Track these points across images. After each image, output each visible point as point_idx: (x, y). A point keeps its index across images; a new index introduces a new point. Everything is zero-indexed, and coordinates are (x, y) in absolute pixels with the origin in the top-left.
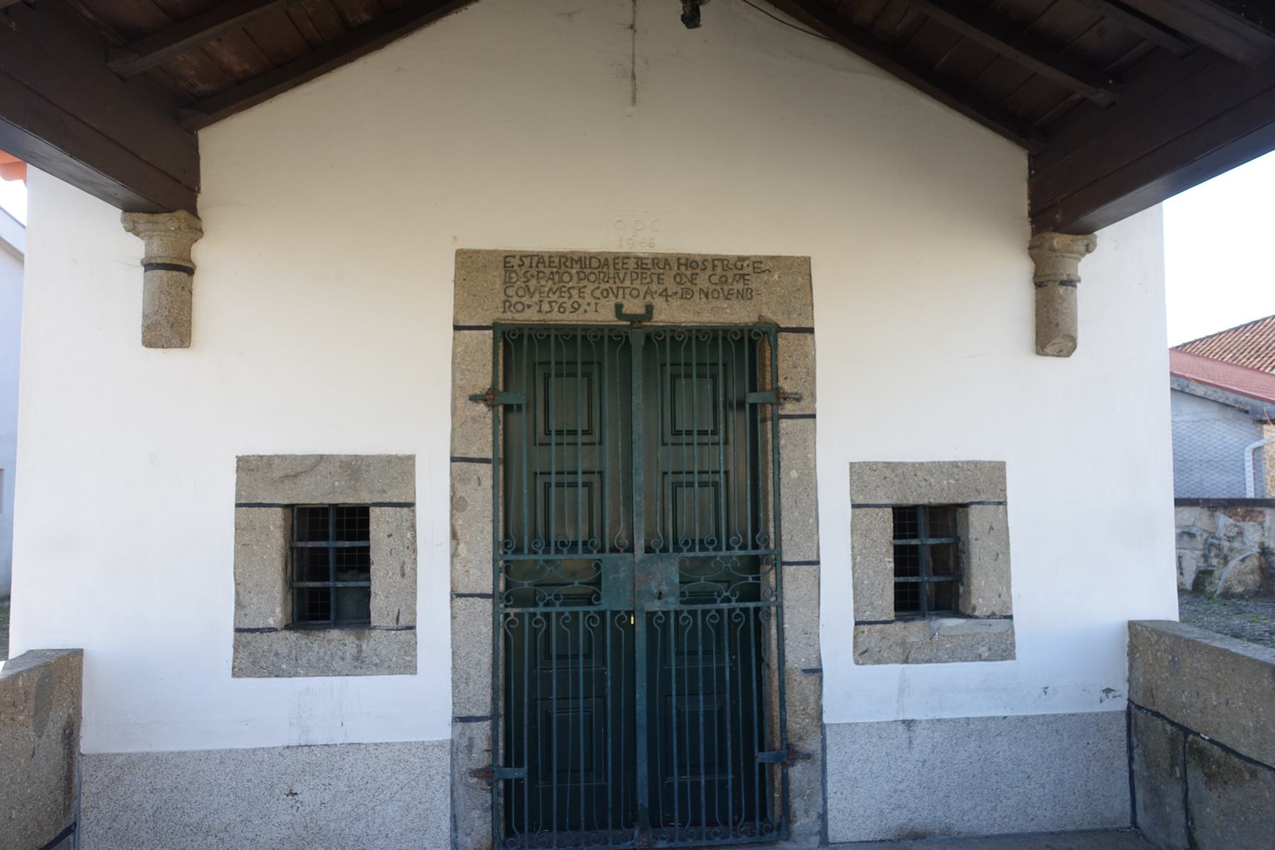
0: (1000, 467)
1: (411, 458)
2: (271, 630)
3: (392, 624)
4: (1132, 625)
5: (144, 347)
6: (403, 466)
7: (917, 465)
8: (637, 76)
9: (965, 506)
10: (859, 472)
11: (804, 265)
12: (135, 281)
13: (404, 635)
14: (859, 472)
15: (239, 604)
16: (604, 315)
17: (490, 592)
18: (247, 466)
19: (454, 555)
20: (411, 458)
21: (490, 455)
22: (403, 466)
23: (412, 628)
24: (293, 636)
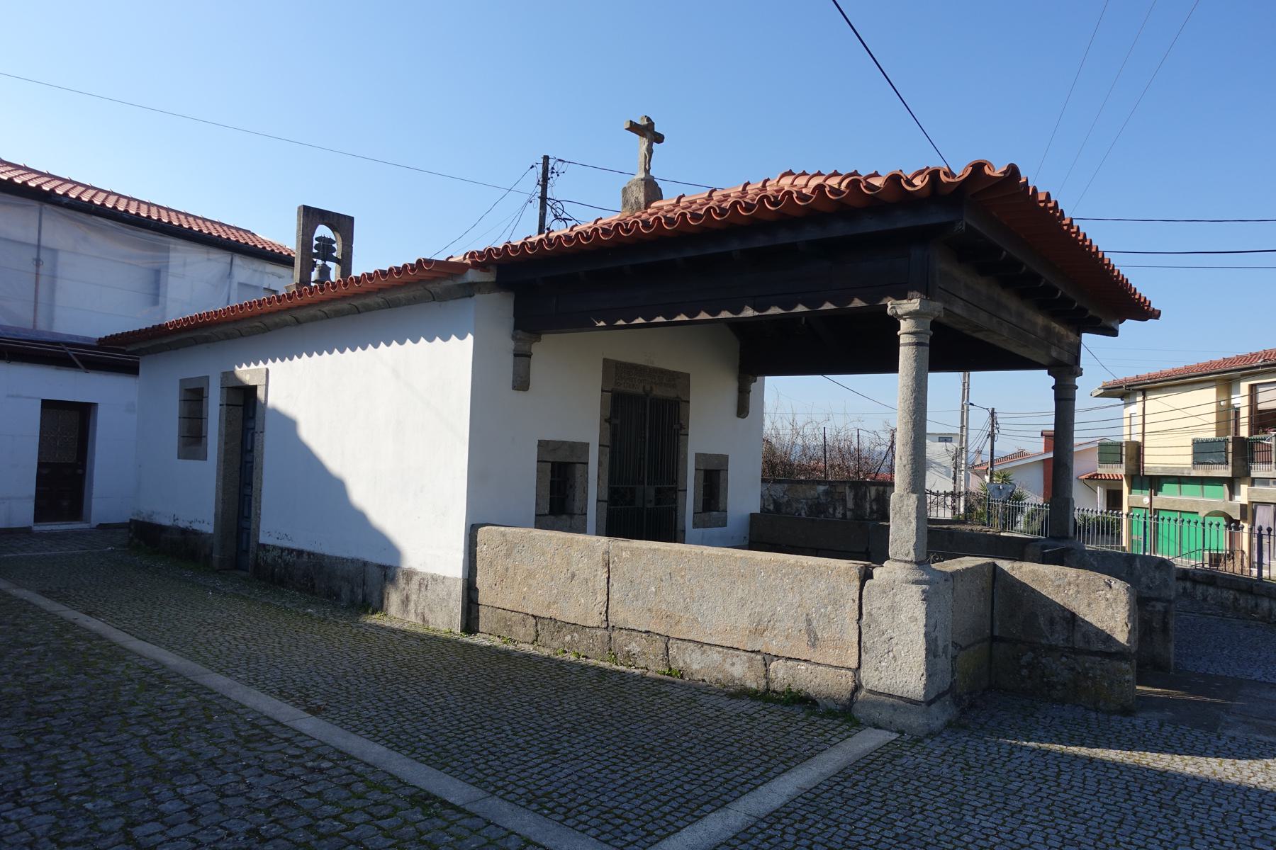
0: (727, 456)
1: (588, 444)
2: (546, 515)
3: (580, 512)
4: (751, 514)
5: (418, 344)
6: (585, 447)
7: (80, 471)
8: (648, 630)
9: (719, 471)
10: (697, 455)
11: (686, 377)
12: (509, 360)
13: (583, 517)
14: (697, 455)
15: (537, 504)
16: (640, 391)
17: (913, 181)
18: (542, 444)
19: (598, 484)
20: (588, 444)
21: (608, 444)
22: (585, 447)
23: (586, 514)
24: (553, 517)
